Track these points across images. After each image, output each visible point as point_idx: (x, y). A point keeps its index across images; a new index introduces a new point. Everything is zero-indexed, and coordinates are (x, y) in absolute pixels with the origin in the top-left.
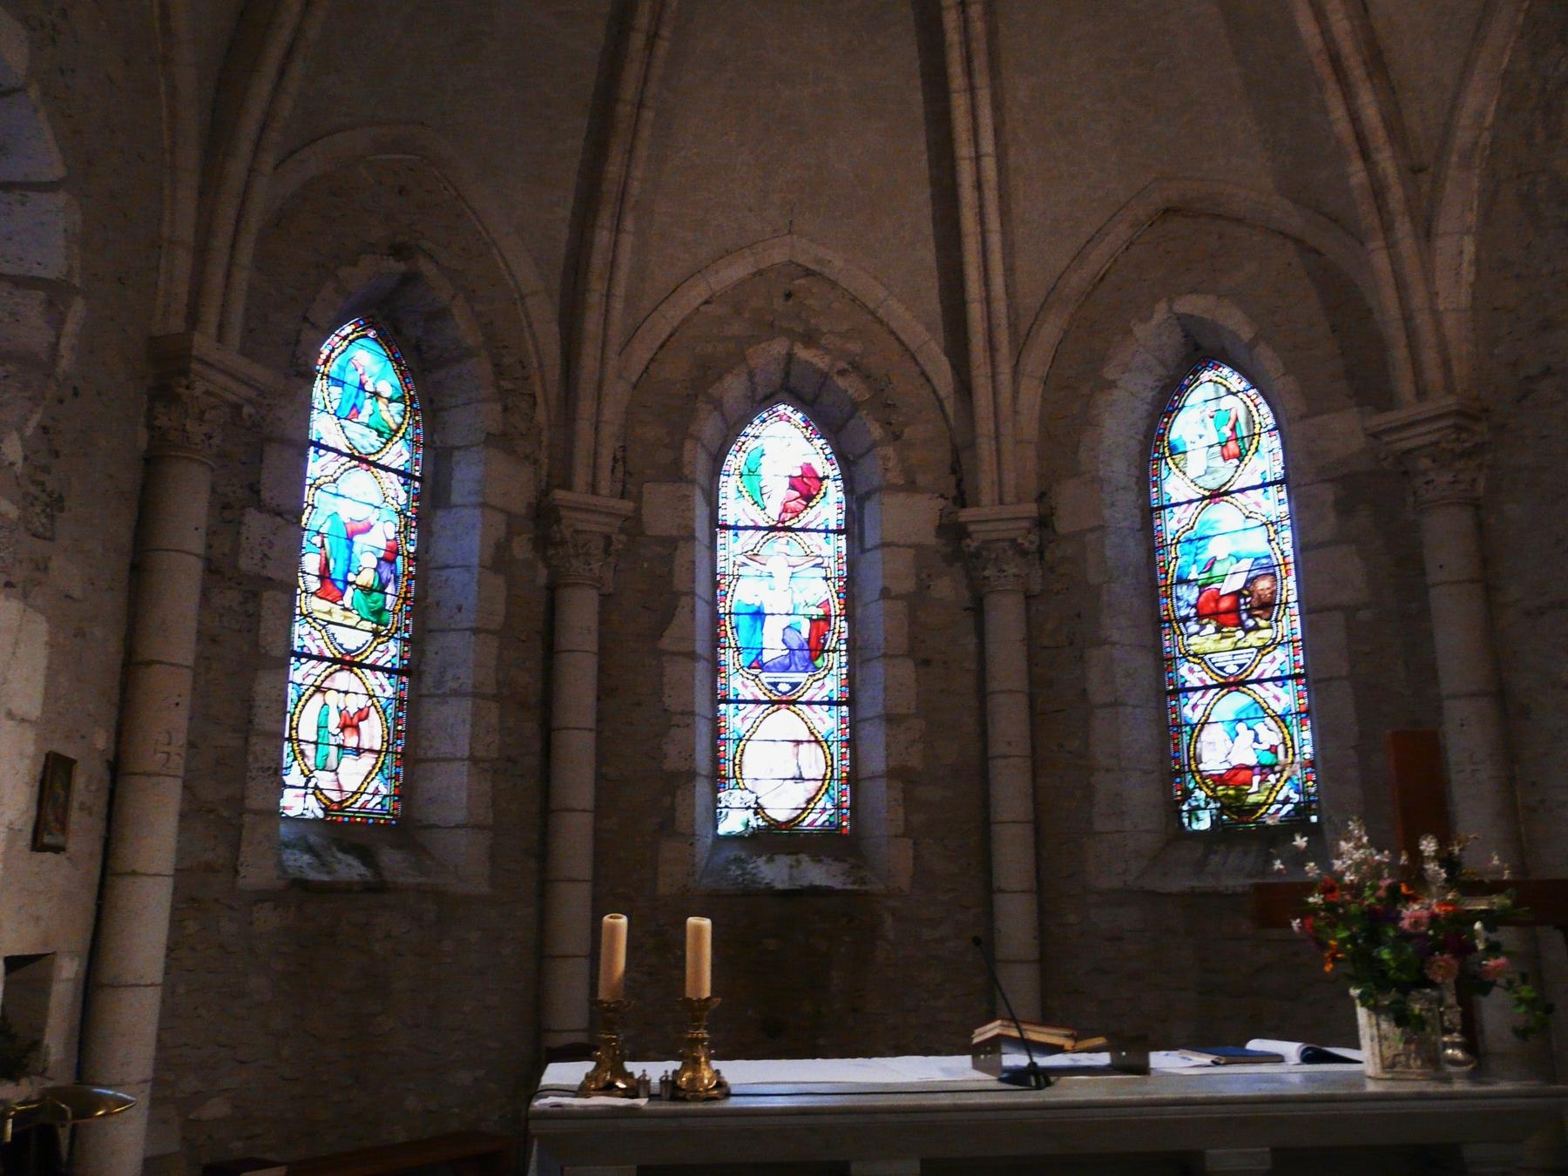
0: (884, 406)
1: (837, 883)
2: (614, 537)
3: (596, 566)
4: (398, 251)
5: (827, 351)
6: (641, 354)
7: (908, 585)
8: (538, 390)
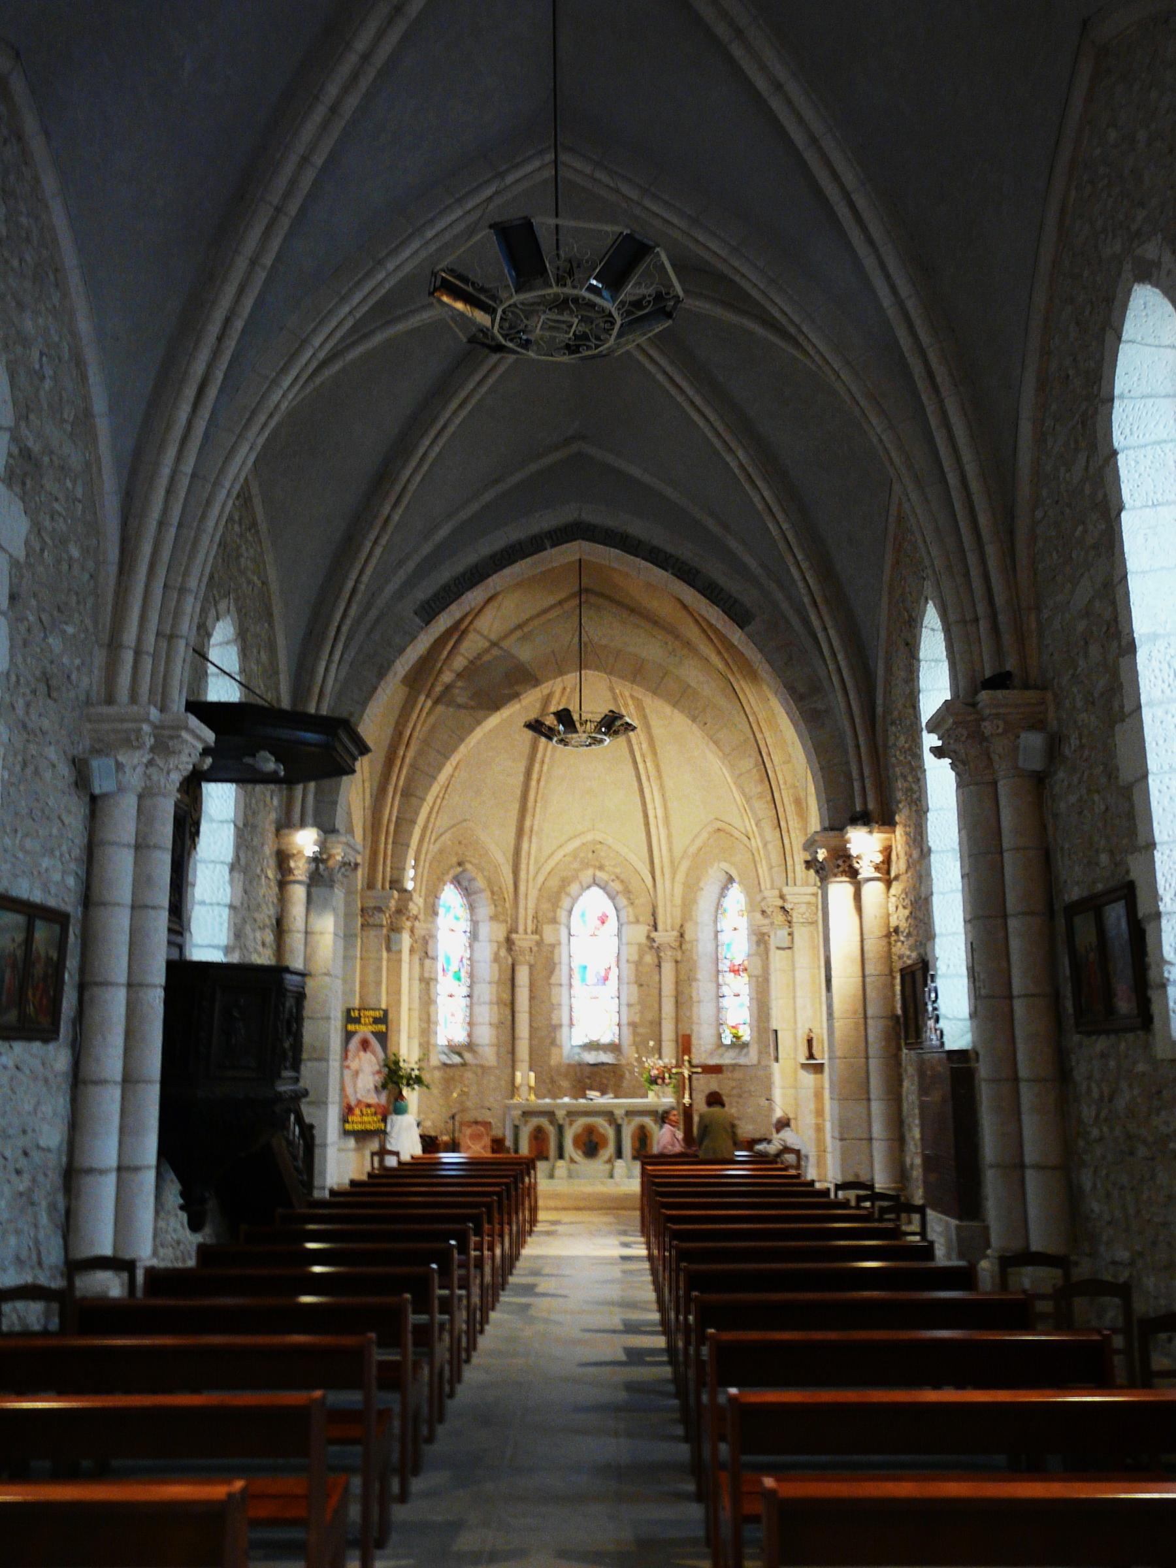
0: (627, 892)
1: (610, 1061)
2: (544, 223)
3: (527, 958)
4: (460, 864)
5: (607, 872)
6: (541, 879)
7: (635, 957)
8: (506, 896)
